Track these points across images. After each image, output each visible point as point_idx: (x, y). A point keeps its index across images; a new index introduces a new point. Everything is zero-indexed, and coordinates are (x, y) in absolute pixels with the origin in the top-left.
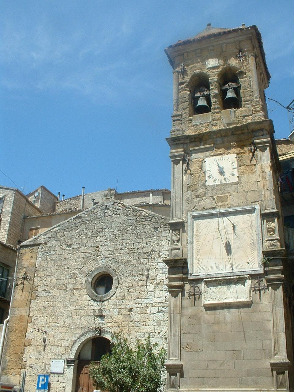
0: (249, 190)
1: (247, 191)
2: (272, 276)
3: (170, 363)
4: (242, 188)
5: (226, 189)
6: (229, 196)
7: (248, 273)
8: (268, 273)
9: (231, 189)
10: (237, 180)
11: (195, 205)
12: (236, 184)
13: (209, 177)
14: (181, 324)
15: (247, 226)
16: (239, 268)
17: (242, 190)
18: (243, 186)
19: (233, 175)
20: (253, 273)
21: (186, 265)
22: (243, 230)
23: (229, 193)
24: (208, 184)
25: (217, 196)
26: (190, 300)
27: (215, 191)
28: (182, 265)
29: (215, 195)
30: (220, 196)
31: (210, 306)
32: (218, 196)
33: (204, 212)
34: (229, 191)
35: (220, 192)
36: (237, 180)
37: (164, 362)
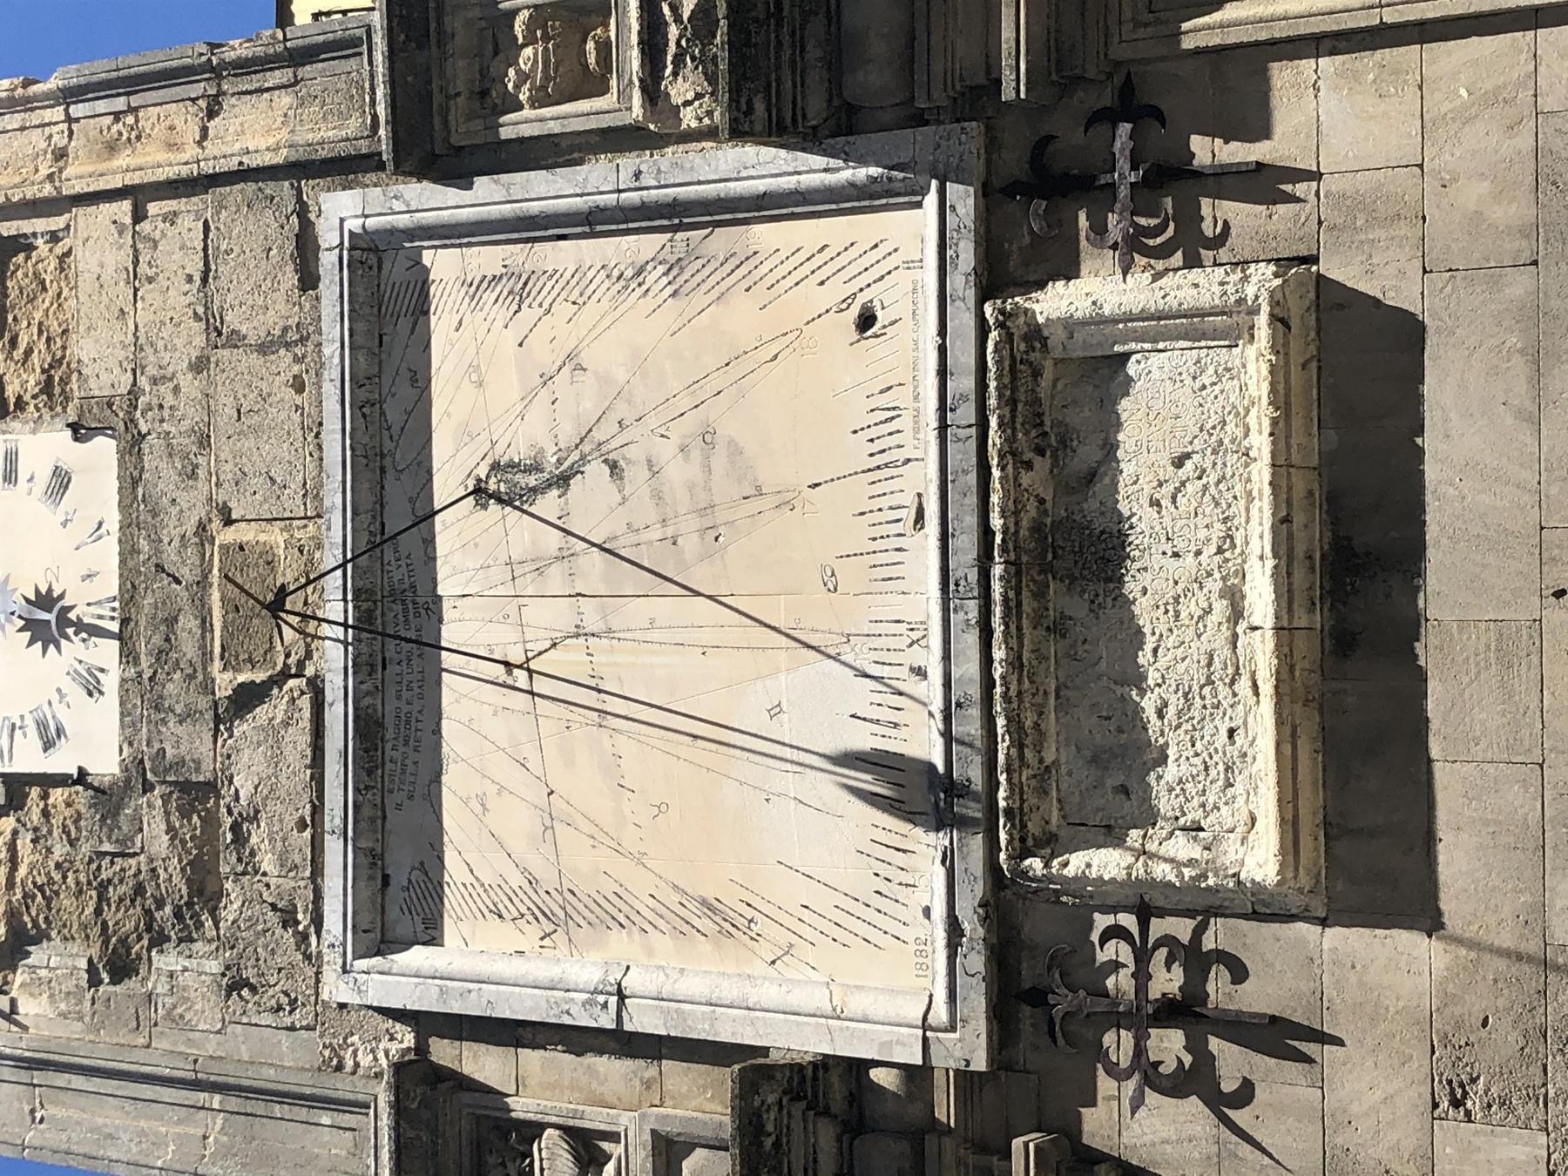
0: (200, 310)
1: (200, 341)
2: (1007, 33)
3: (1335, 274)
4: (176, 390)
5: (170, 556)
6: (228, 536)
7: (963, 320)
8: (981, 80)
9: (174, 511)
10: (104, 449)
11: (272, 918)
12: (132, 446)
13: (48, 745)
14: (812, 768)
15: (511, 337)
16: (908, 433)
17: (190, 385)
18: (154, 381)
19: (61, 481)
20: (966, 255)
21: (834, 1077)
22: (546, 379)
23: (202, 527)
24: (106, 763)
25: (217, 664)
26: (1260, 1093)
27: (173, 687)
28: (826, 1136)
29: (208, 687)
30: (217, 633)
31: (1310, 803)
32: (217, 650)
33: (338, 821)
34: (190, 526)
35: (188, 623)
36: (104, 449)
37: (1216, 916)
